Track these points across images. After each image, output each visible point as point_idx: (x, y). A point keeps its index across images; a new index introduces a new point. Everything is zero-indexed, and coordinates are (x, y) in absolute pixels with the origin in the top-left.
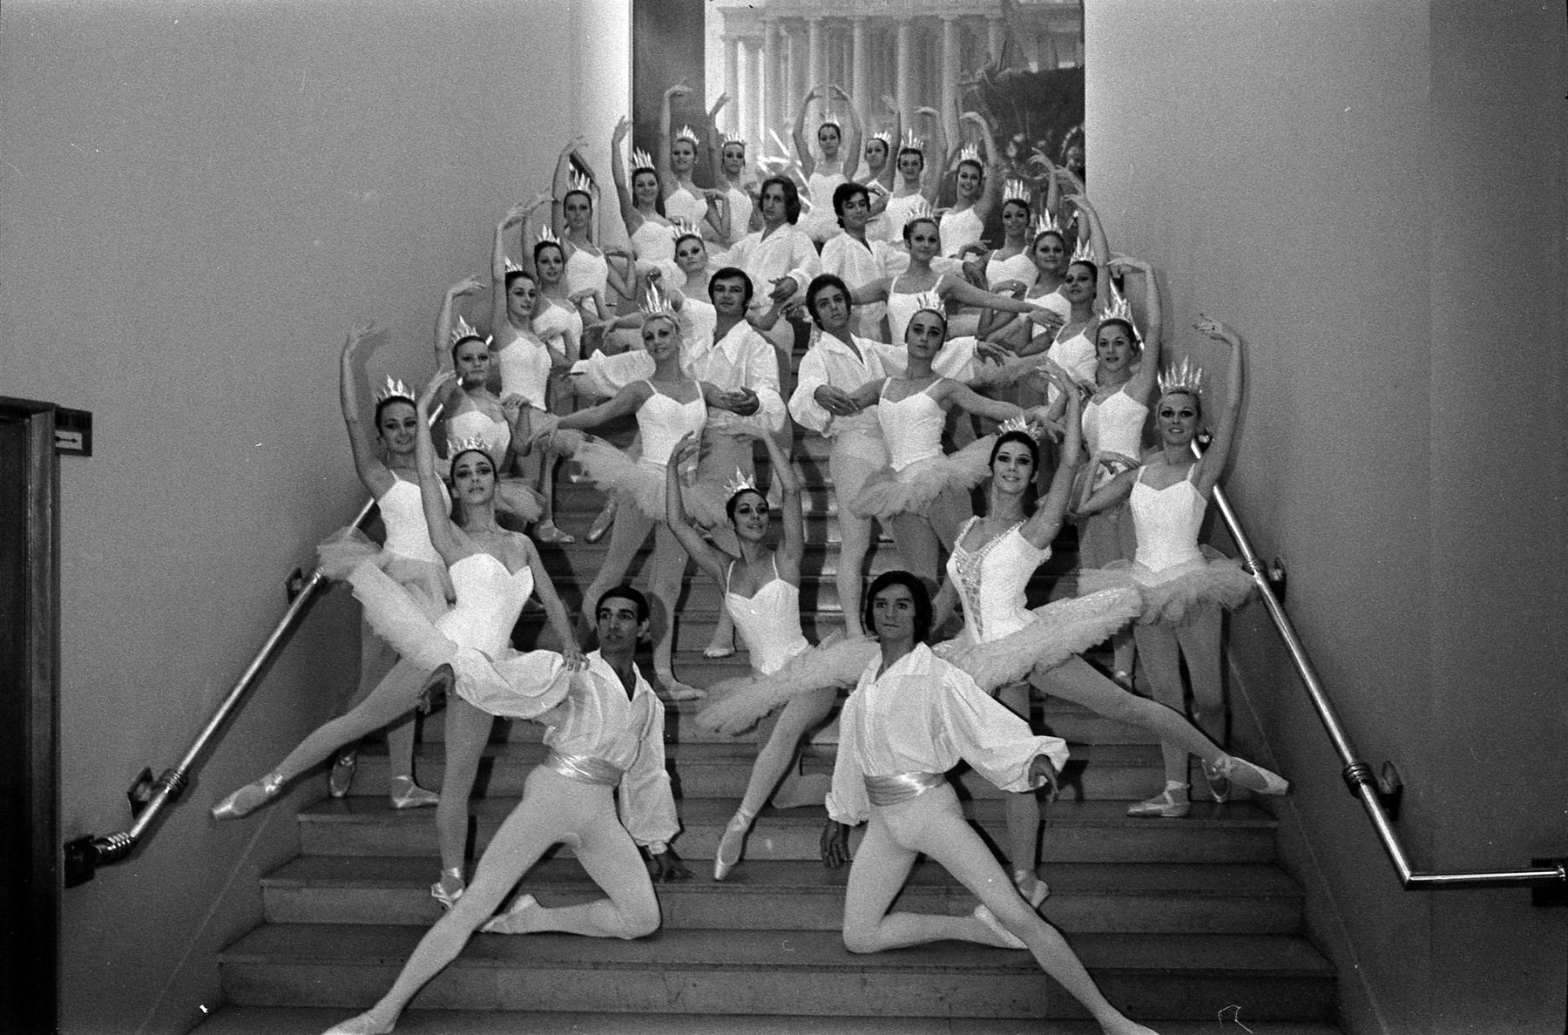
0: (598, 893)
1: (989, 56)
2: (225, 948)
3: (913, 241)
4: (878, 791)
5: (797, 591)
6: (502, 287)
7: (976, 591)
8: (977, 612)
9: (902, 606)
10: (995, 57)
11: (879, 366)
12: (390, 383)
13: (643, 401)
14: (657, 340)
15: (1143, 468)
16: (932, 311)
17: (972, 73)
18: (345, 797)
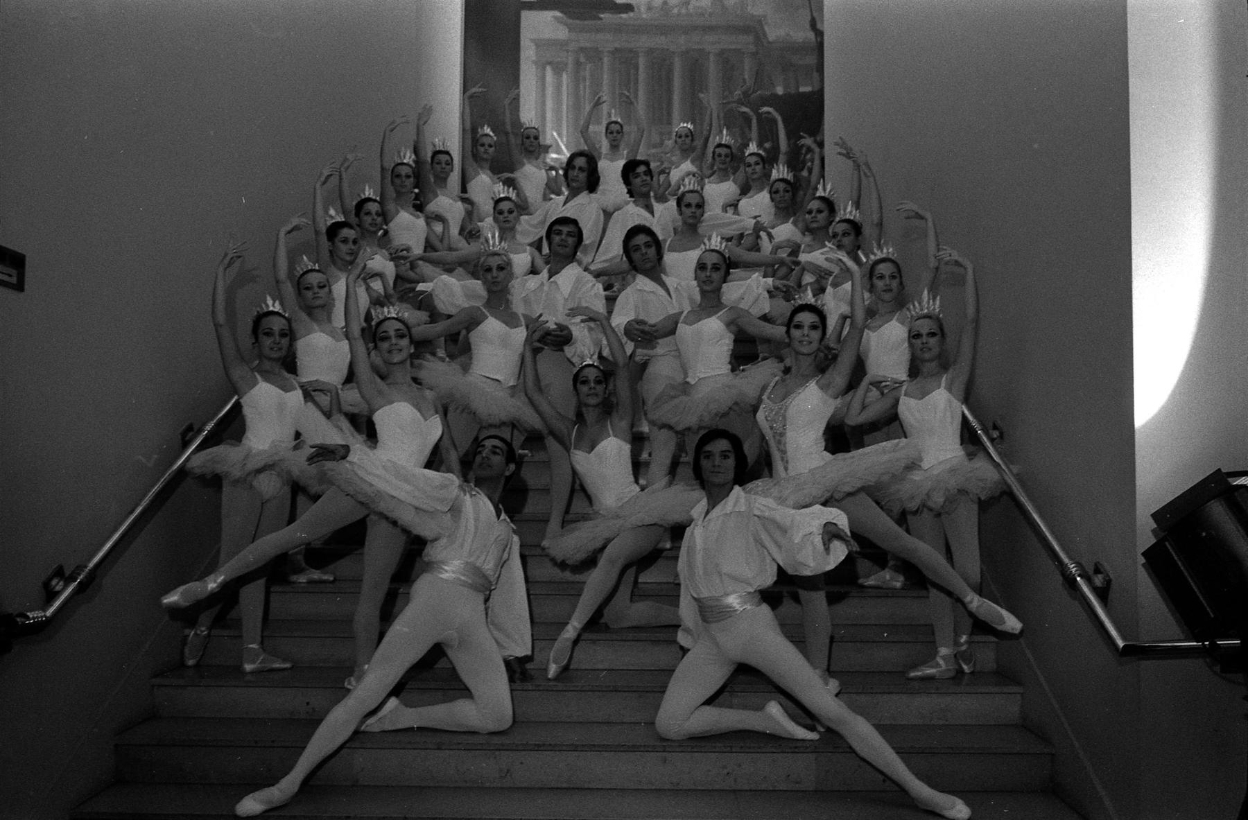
0: (464, 692)
1: (744, 80)
3: (684, 209)
6: (324, 238)
7: (782, 435)
8: (784, 452)
10: (750, 82)
12: (270, 302)
13: (478, 324)
14: (495, 272)
16: (713, 251)
17: (731, 93)
18: (197, 666)
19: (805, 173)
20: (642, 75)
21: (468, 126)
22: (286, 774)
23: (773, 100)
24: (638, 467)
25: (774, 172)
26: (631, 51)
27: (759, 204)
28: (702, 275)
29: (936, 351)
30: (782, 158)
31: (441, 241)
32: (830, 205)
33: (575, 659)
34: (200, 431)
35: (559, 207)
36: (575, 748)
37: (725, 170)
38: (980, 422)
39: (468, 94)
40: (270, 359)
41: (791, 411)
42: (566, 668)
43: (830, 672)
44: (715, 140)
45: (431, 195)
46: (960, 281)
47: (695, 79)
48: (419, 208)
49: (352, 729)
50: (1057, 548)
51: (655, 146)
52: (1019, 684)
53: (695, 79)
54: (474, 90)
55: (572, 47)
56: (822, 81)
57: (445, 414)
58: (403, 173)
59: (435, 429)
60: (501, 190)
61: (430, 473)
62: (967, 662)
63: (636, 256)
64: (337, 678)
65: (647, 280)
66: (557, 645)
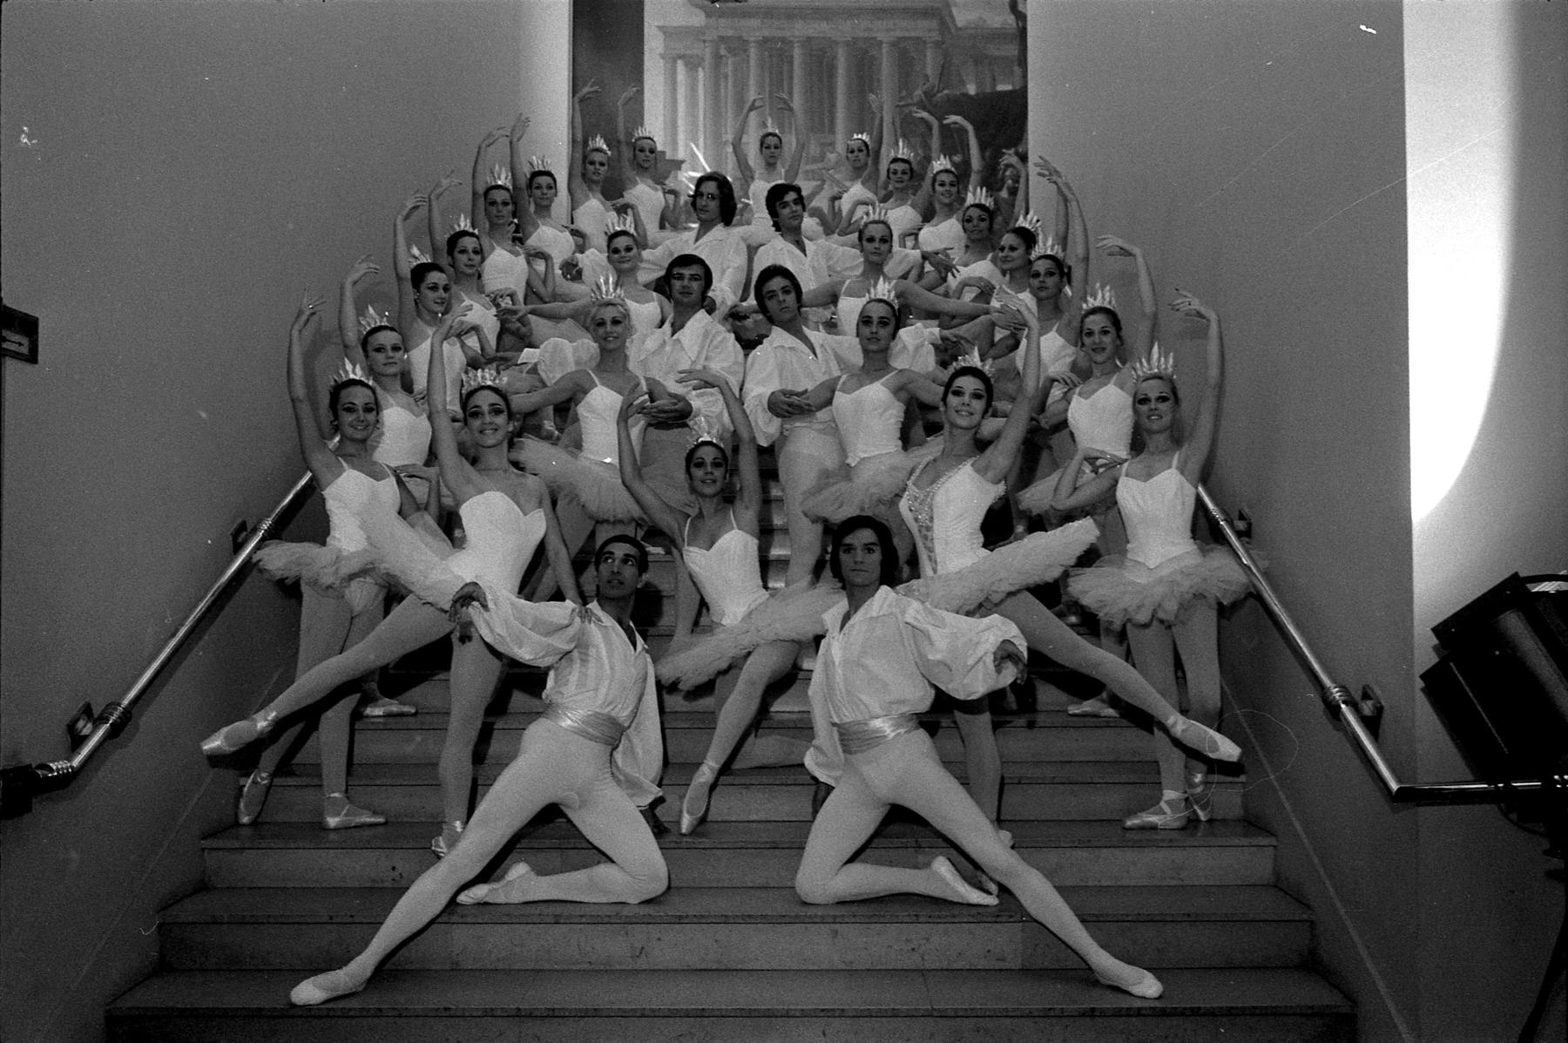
1: (926, 76)
2: (165, 909)
4: (852, 739)
5: (756, 541)
6: (408, 286)
7: (929, 529)
8: (931, 550)
9: (870, 551)
11: (833, 364)
12: (349, 367)
13: (586, 392)
14: (609, 327)
15: (1126, 465)
17: (910, 95)
18: (254, 824)
19: (1004, 194)
20: (798, 71)
21: (579, 137)
22: (359, 953)
23: (959, 104)
24: (766, 566)
25: (970, 195)
26: (783, 40)
27: (944, 234)
28: (866, 331)
29: (1167, 419)
30: (974, 178)
31: (544, 282)
32: (1028, 238)
33: (712, 808)
34: (255, 530)
35: (684, 241)
36: (726, 920)
37: (902, 190)
38: (1224, 511)
39: (579, 95)
40: (353, 440)
41: (940, 498)
42: (703, 820)
43: (999, 822)
44: (887, 154)
45: (530, 228)
46: (1202, 333)
47: (864, 78)
48: (519, 239)
49: (443, 900)
50: (1316, 667)
51: (815, 161)
52: (1270, 833)
53: (864, 78)
54: (586, 90)
55: (711, 35)
56: (1025, 76)
57: (554, 503)
58: (499, 200)
59: (537, 525)
60: (614, 222)
61: (1005, 551)
62: (1203, 808)
63: (772, 305)
64: (418, 838)
65: (786, 335)
66: (690, 793)
